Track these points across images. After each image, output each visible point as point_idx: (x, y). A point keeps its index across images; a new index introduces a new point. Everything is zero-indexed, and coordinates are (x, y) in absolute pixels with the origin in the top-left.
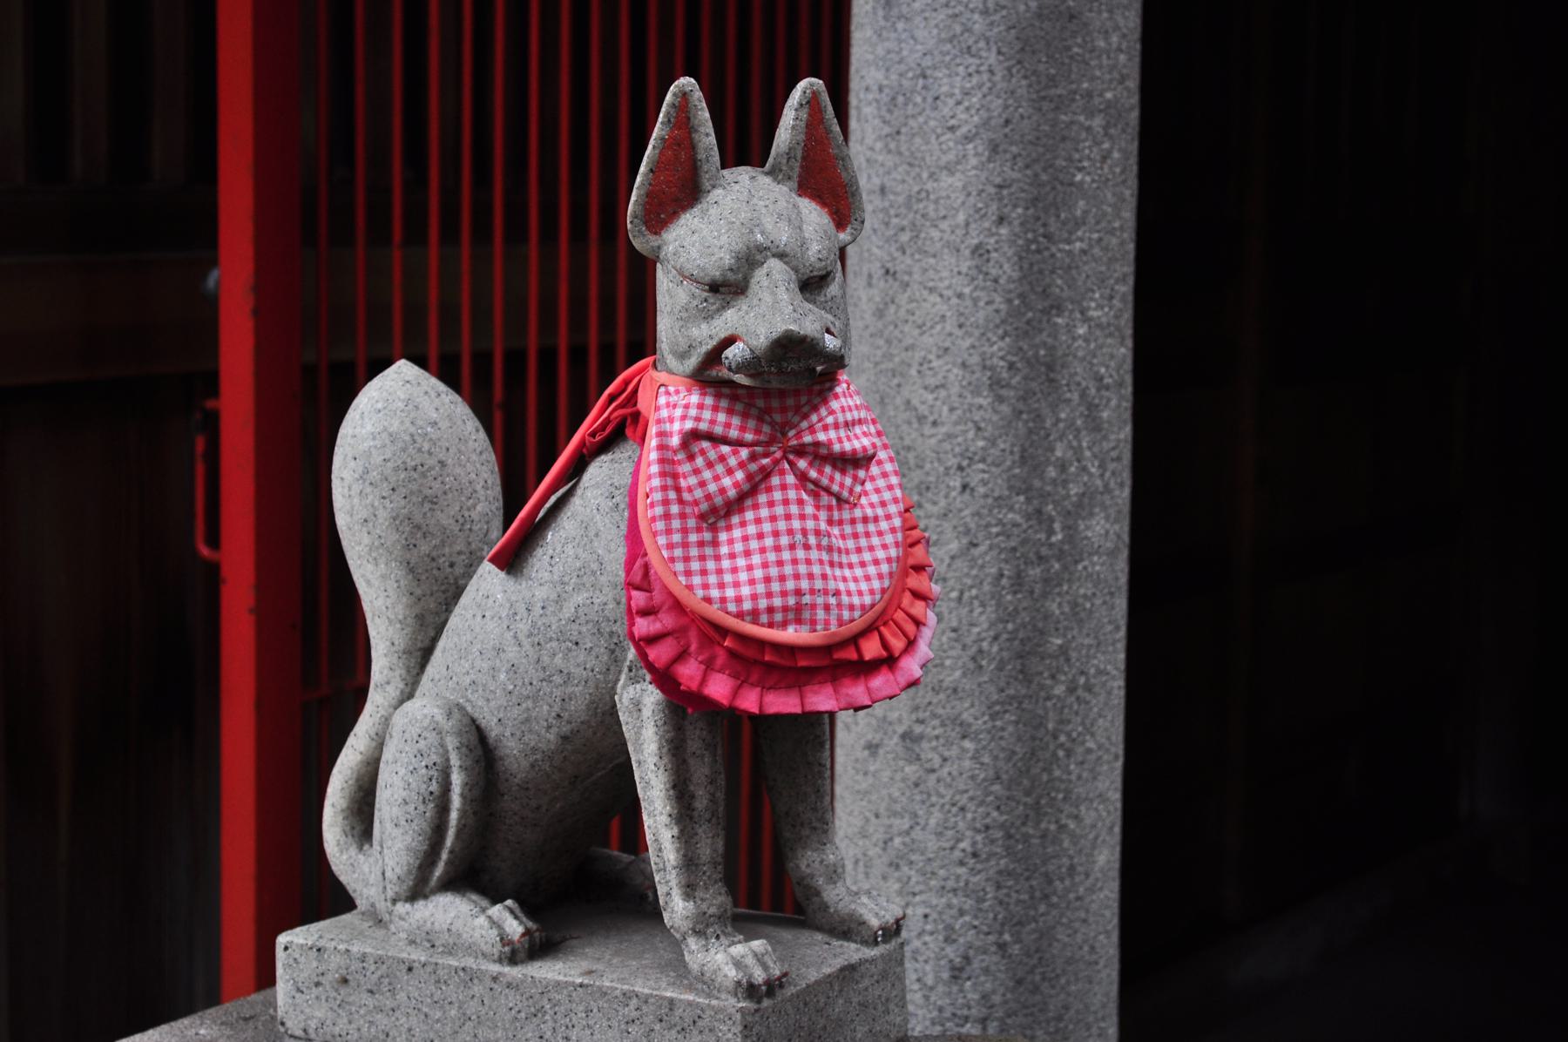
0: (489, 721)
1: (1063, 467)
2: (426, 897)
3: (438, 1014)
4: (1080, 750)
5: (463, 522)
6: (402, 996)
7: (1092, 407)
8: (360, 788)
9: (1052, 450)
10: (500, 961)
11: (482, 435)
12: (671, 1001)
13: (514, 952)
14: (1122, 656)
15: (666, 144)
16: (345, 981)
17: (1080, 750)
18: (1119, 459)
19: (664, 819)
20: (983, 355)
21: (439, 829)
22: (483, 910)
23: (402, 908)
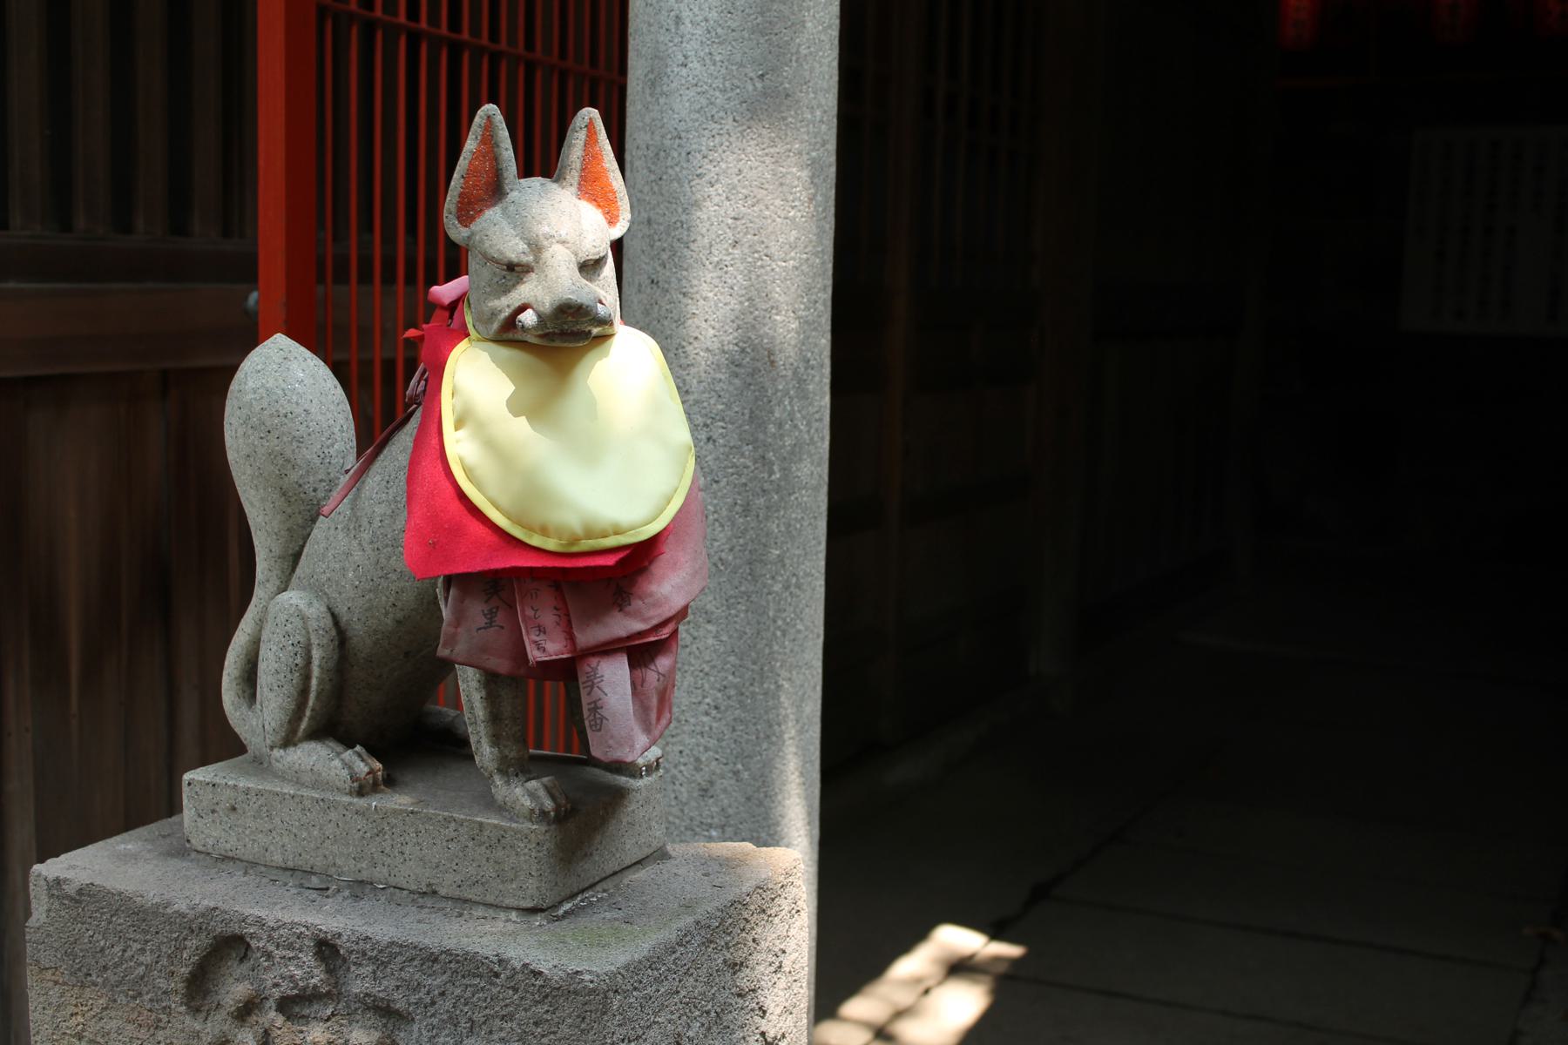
0: (342, 610)
1: (780, 425)
2: (295, 745)
3: (305, 835)
4: (793, 631)
5: (323, 457)
6: (277, 820)
7: (801, 381)
8: (249, 662)
9: (772, 412)
10: (350, 794)
11: (340, 390)
12: (481, 824)
13: (361, 787)
14: (823, 563)
15: (476, 155)
16: (234, 809)
17: (793, 631)
18: (820, 420)
19: (474, 684)
20: (721, 342)
21: (304, 692)
22: (338, 754)
23: (277, 753)
